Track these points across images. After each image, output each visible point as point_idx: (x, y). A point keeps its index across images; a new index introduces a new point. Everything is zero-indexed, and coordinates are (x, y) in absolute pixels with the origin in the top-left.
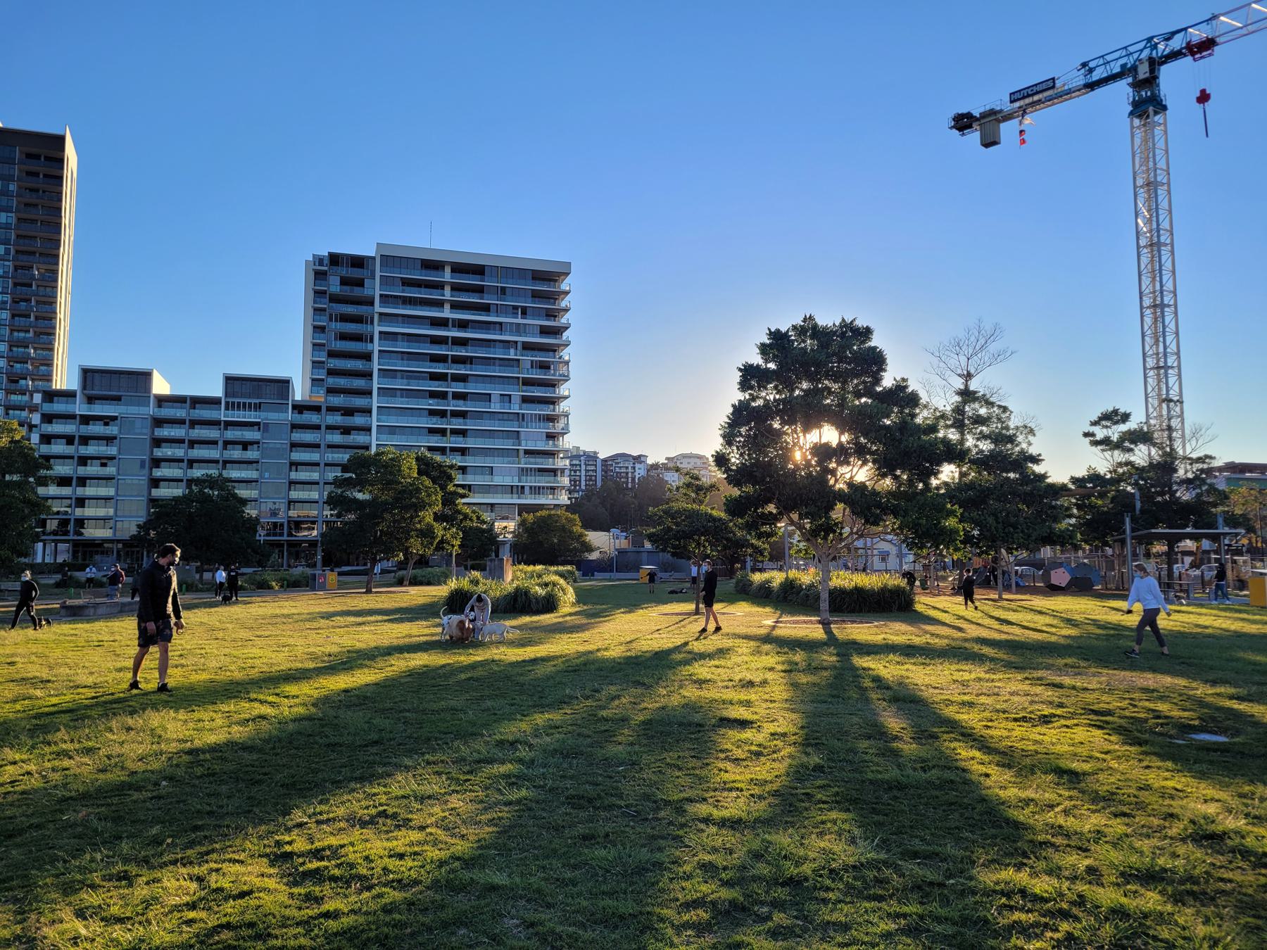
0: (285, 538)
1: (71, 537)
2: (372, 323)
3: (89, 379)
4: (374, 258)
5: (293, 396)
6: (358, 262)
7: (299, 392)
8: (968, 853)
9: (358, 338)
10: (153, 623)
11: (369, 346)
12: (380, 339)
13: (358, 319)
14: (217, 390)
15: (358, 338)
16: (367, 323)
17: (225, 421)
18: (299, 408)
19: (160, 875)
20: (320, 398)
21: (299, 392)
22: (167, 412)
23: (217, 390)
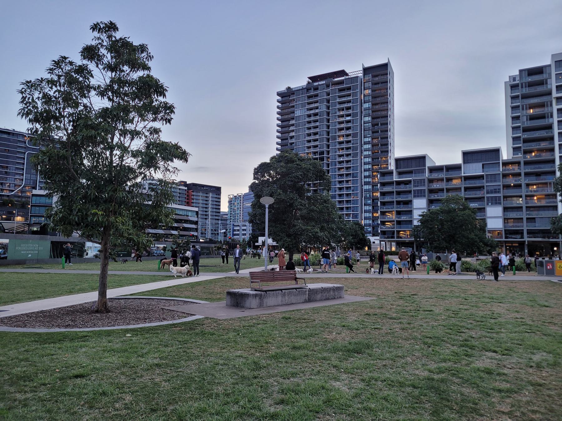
0: (504, 239)
1: (395, 239)
2: (551, 105)
3: (398, 163)
4: (550, 66)
5: (502, 157)
6: (539, 71)
7: (505, 155)
8: (100, 41)
9: (543, 117)
10: (455, 255)
11: (551, 120)
12: (558, 114)
13: (542, 105)
14: (458, 160)
15: (543, 117)
16: (547, 106)
17: (464, 176)
18: (505, 164)
19: (478, 267)
20: (520, 156)
21: (505, 155)
22: (435, 175)
23: (458, 160)
